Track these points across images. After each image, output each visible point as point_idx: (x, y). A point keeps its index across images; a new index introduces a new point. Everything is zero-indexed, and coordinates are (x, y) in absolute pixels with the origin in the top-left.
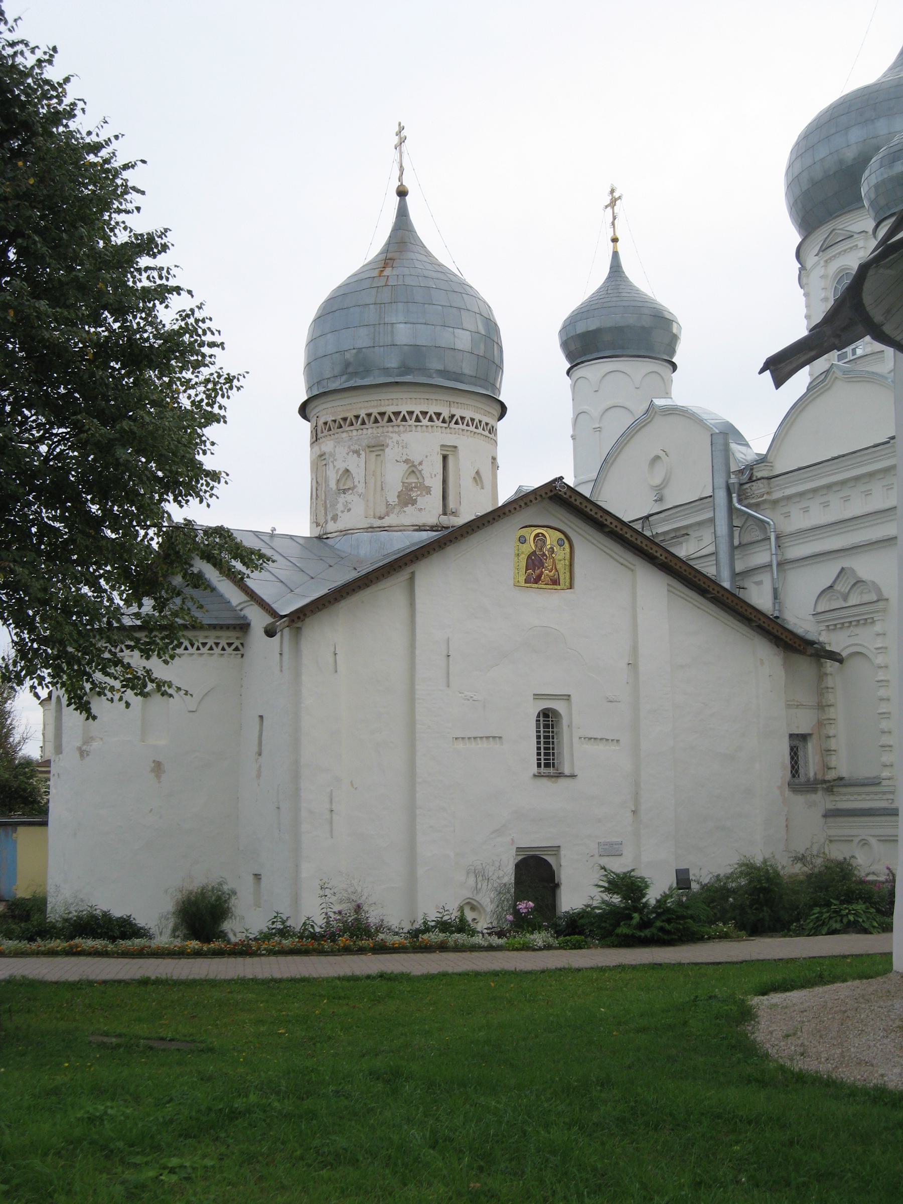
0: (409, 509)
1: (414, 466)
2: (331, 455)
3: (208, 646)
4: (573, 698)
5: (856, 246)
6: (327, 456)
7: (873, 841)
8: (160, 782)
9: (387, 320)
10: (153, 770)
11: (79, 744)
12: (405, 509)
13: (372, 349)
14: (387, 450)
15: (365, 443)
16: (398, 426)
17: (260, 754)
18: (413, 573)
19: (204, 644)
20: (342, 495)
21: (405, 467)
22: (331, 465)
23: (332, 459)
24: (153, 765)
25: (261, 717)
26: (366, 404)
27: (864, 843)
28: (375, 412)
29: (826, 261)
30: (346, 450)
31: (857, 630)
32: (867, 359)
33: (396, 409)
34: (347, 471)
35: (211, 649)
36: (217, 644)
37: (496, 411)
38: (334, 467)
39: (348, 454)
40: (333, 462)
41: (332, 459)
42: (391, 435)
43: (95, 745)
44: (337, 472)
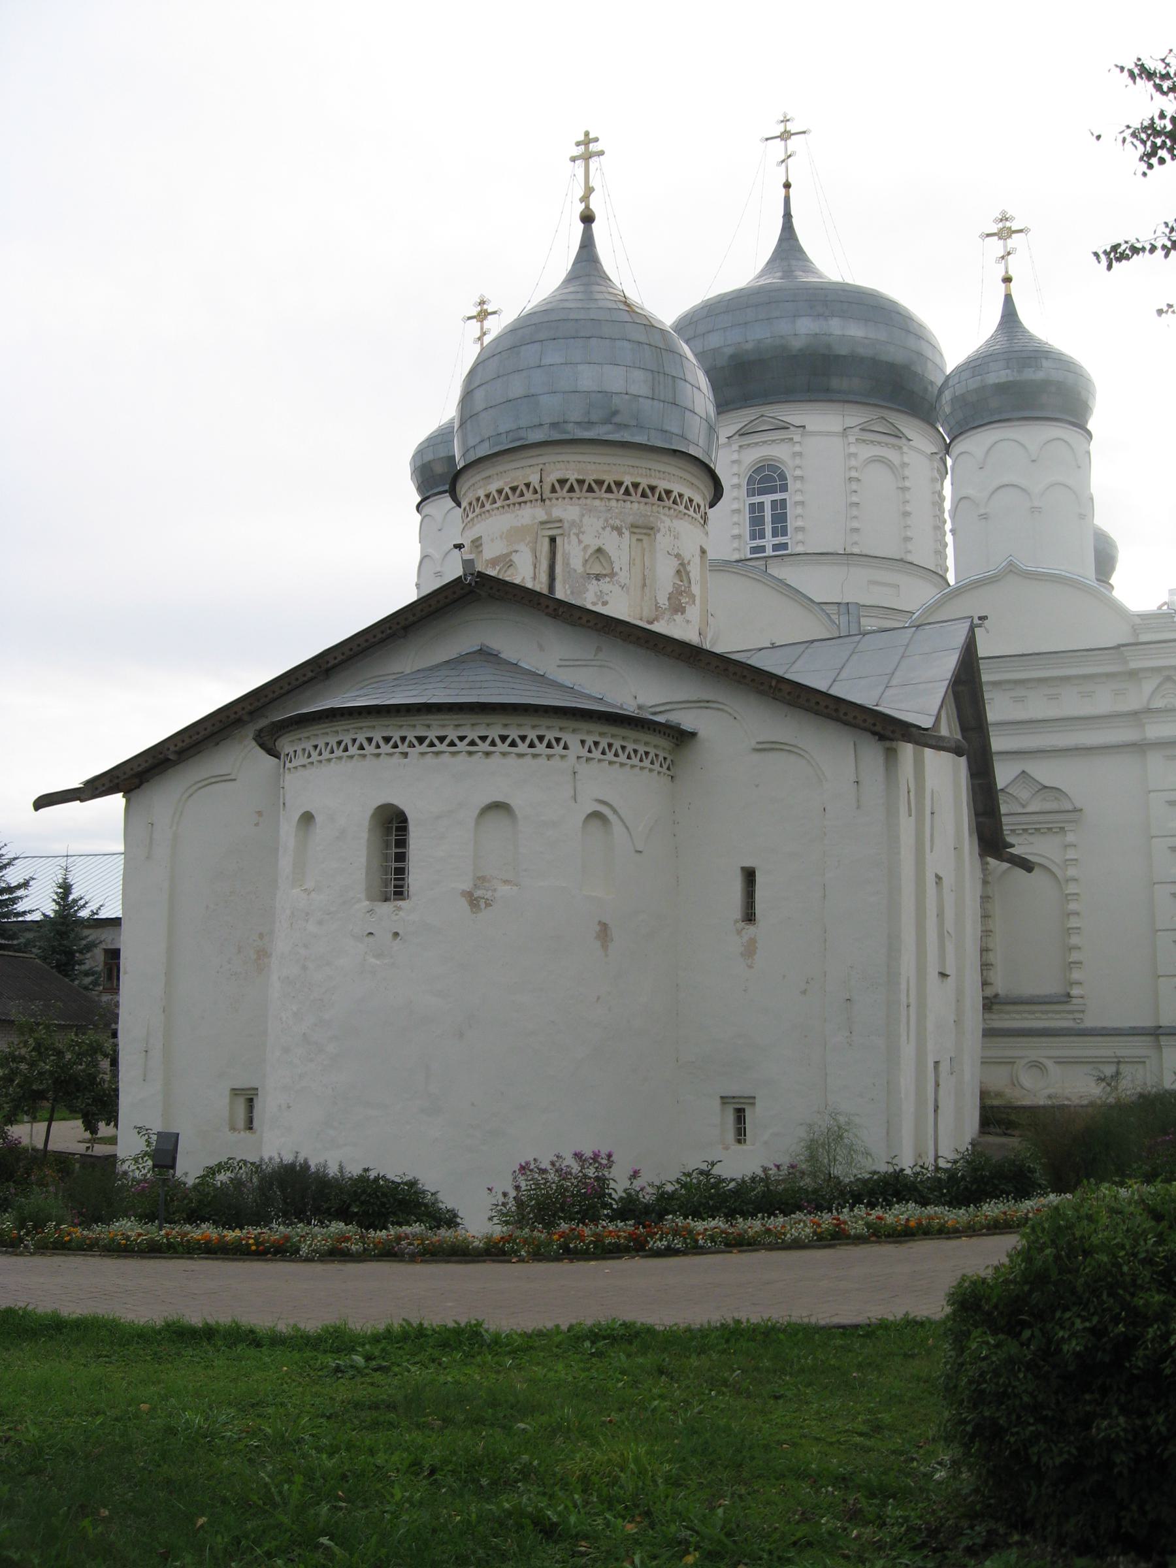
0: (678, 617)
1: (682, 564)
2: (573, 524)
6: (566, 525)
7: (1049, 1064)
11: (467, 886)
12: (675, 617)
13: (650, 401)
14: (659, 536)
15: (630, 519)
16: (670, 508)
17: (749, 916)
20: (594, 582)
23: (575, 530)
25: (750, 876)
26: (632, 470)
27: (1037, 1065)
28: (644, 482)
29: (740, 447)
30: (601, 523)
31: (1031, 839)
32: (799, 558)
34: (599, 550)
38: (580, 542)
39: (604, 528)
40: (577, 535)
41: (575, 530)
44: (586, 548)
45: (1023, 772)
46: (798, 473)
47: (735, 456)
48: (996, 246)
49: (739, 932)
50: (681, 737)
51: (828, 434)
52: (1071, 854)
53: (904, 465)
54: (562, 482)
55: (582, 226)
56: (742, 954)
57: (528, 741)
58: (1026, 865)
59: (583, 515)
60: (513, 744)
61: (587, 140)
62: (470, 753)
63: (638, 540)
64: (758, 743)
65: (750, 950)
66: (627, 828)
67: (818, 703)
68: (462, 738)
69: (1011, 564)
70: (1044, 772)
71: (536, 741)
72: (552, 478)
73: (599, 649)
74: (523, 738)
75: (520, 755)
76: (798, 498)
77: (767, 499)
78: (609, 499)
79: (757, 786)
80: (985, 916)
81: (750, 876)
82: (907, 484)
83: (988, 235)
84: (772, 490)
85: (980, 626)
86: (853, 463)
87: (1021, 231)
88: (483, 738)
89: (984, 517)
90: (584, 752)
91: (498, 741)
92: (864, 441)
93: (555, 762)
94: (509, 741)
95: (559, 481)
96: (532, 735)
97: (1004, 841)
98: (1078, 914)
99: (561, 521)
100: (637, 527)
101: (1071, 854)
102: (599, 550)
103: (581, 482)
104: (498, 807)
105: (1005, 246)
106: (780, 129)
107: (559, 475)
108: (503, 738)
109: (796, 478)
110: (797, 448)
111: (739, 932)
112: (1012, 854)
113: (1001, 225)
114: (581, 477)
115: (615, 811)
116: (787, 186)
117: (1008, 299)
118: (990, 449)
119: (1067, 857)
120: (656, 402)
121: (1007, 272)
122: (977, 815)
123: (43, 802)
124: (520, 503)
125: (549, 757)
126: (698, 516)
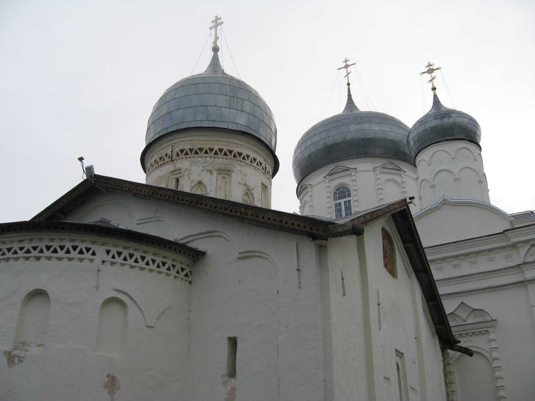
1: (249, 189)
2: (186, 170)
3: (166, 266)
5: (351, 174)
6: (183, 171)
10: (106, 386)
11: (7, 348)
13: (228, 109)
14: (233, 175)
15: (217, 166)
16: (241, 161)
17: (232, 373)
19: (164, 264)
21: (244, 188)
22: (186, 178)
23: (187, 173)
24: (106, 380)
25: (233, 342)
26: (219, 142)
28: (225, 148)
30: (201, 168)
31: (471, 338)
34: (200, 183)
36: (174, 266)
38: (189, 179)
39: (202, 171)
40: (188, 176)
41: (187, 173)
42: (236, 166)
43: (33, 350)
44: (192, 182)
45: (462, 302)
46: (355, 188)
47: (328, 185)
48: (428, 77)
49: (225, 384)
50: (197, 256)
51: (366, 171)
52: (493, 345)
53: (403, 182)
54: (182, 151)
55: (212, 53)
57: (65, 249)
58: (468, 352)
59: (192, 165)
60: (55, 251)
61: (217, 19)
62: (27, 258)
64: (240, 253)
66: (141, 310)
67: (269, 219)
68: (21, 249)
69: (444, 200)
70: (474, 302)
71: (71, 250)
72: (177, 149)
74: (62, 248)
75: (60, 259)
76: (356, 198)
77: (342, 201)
78: (206, 157)
79: (240, 282)
80: (448, 384)
81: (233, 342)
82: (405, 190)
83: (423, 73)
84: (344, 197)
85: (411, 203)
86: (379, 182)
87: (438, 69)
88: (35, 248)
89: (433, 186)
90: (109, 258)
91: (45, 249)
92: (384, 173)
93: (86, 263)
94: (52, 249)
95: (180, 151)
96: (69, 245)
97: (454, 339)
98: (502, 378)
99: (180, 169)
100: (222, 171)
101: (493, 345)
102: (200, 183)
103: (191, 150)
104: (39, 294)
105: (431, 76)
106: (349, 69)
107: (180, 148)
108: (48, 248)
110: (354, 178)
111: (225, 384)
112: (459, 346)
113: (428, 68)
114: (191, 147)
115: (131, 298)
116: (349, 84)
117: (435, 96)
118: (433, 155)
119: (492, 347)
120: (232, 110)
121: (433, 86)
122: (435, 324)
124: (163, 165)
125: (81, 260)
126: (261, 168)
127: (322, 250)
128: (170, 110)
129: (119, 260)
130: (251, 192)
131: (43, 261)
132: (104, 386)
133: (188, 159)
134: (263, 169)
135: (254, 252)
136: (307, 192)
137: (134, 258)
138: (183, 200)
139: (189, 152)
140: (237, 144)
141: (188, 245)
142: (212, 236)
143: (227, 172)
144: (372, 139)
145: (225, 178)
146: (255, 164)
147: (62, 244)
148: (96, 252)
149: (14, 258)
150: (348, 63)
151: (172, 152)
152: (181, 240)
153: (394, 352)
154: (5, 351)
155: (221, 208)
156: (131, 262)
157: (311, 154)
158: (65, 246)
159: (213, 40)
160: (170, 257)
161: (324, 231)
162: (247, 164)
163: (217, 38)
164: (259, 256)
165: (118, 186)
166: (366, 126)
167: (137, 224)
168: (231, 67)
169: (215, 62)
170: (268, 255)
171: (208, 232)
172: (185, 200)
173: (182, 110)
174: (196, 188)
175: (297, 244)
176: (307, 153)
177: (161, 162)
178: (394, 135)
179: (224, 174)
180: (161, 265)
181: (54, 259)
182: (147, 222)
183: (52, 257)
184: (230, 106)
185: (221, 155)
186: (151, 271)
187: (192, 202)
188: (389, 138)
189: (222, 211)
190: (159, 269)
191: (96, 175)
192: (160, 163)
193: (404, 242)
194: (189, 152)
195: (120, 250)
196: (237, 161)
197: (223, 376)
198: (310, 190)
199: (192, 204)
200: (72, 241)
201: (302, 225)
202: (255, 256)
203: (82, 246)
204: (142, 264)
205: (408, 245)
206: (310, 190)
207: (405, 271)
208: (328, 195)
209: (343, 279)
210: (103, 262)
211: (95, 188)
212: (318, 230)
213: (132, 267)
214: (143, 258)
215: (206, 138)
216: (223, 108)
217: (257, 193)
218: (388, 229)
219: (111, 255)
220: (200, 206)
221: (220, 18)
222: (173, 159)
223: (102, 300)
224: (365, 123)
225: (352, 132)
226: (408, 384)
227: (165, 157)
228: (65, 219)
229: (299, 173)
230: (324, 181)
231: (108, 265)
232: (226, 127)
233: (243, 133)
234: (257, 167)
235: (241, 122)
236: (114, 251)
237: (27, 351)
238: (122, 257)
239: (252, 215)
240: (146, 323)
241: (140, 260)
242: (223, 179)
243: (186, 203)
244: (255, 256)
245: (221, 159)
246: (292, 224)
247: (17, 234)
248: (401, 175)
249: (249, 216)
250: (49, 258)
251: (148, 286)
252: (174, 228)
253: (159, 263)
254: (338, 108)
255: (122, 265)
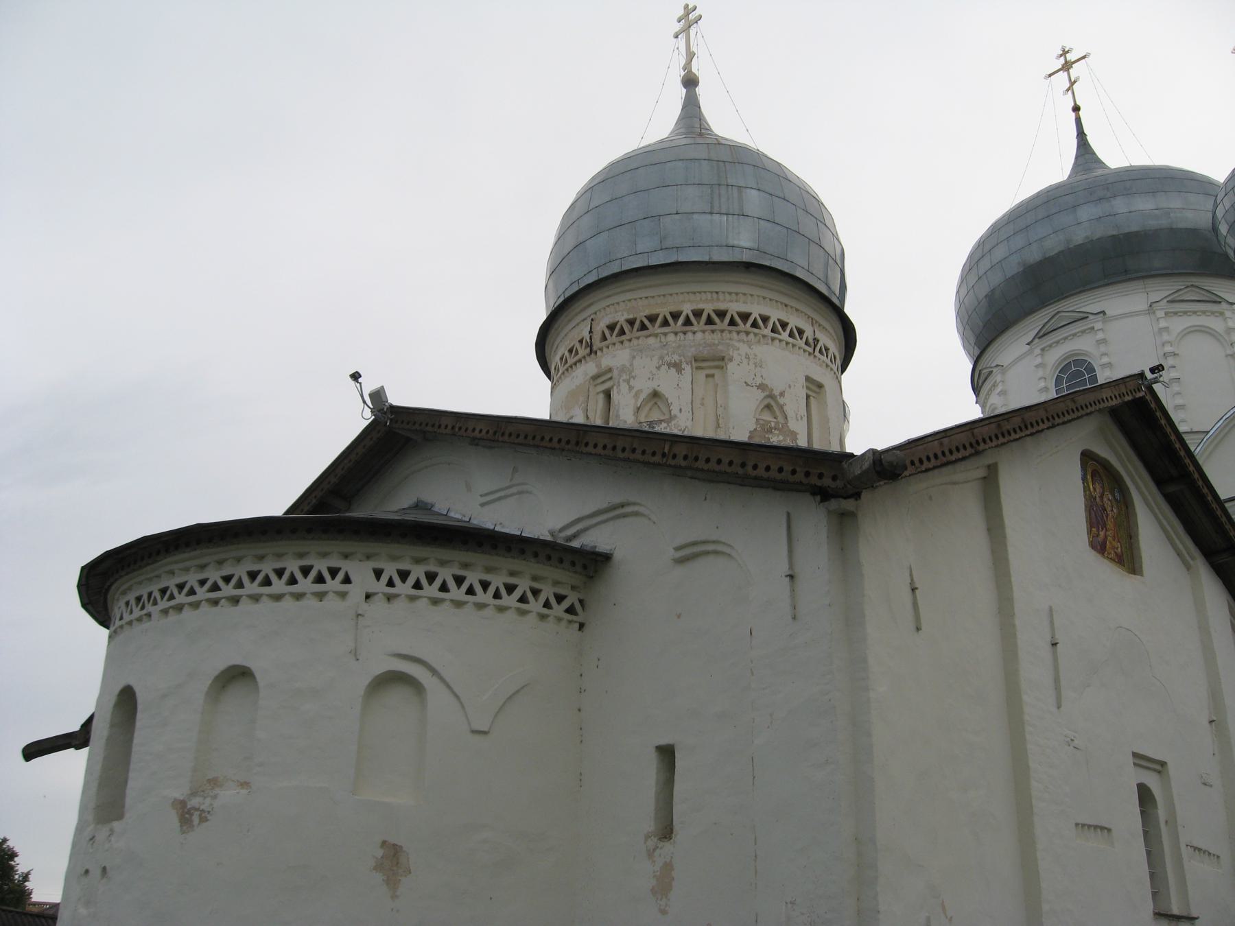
1: (771, 396)
2: (623, 369)
3: (517, 594)
4: (1171, 767)
5: (1093, 328)
6: (615, 373)
8: (394, 897)
9: (730, 181)
10: (379, 867)
11: (178, 795)
13: (708, 216)
14: (731, 367)
15: (691, 352)
16: (747, 333)
17: (666, 832)
18: (993, 470)
19: (510, 589)
21: (760, 395)
23: (625, 377)
25: (667, 754)
26: (692, 297)
28: (709, 308)
30: (655, 361)
33: (744, 308)
34: (655, 394)
35: (523, 599)
36: (536, 592)
37: (830, 341)
38: (631, 388)
39: (658, 368)
40: (628, 381)
41: (625, 377)
42: (737, 344)
43: (228, 795)
44: (637, 395)
46: (1105, 360)
47: (1039, 360)
50: (592, 564)
54: (611, 327)
56: (653, 891)
57: (286, 576)
59: (634, 357)
60: (267, 582)
61: (688, 10)
63: (707, 376)
64: (677, 549)
65: (663, 884)
71: (299, 576)
72: (601, 326)
73: (515, 470)
75: (278, 598)
78: (665, 334)
79: (679, 616)
81: (667, 754)
85: (1156, 381)
86: (1166, 337)
88: (227, 579)
90: (381, 586)
91: (246, 580)
92: (1176, 313)
93: (332, 602)
96: (293, 566)
99: (610, 370)
102: (655, 394)
103: (631, 322)
104: (237, 676)
106: (1074, 72)
107: (607, 320)
109: (1104, 366)
110: (1100, 336)
111: (650, 854)
114: (631, 316)
115: (434, 671)
116: (1076, 109)
120: (716, 217)
123: (33, 751)
126: (801, 343)
127: (844, 524)
128: (581, 239)
129: (404, 588)
130: (776, 402)
131: (246, 605)
132: (375, 868)
133: (626, 344)
134: (807, 343)
135: (704, 542)
136: (995, 385)
137: (438, 583)
138: (551, 440)
139: (626, 328)
140: (737, 294)
141: (576, 544)
142: (625, 516)
143: (716, 363)
144: (1136, 234)
145: (713, 376)
146: (785, 335)
147: (278, 565)
148: (352, 578)
149: (191, 604)
150: (1069, 57)
151: (591, 332)
152: (561, 530)
153: (1131, 760)
154: (175, 800)
155: (624, 450)
156: (432, 590)
157: (993, 291)
158: (284, 569)
159: (683, 62)
160: (525, 575)
161: (834, 478)
162: (764, 336)
163: (691, 56)
164: (716, 552)
165: (433, 426)
166: (1120, 205)
167: (482, 505)
168: (726, 121)
169: (691, 110)
170: (729, 546)
171: (614, 508)
172: (555, 440)
173: (604, 235)
174: (647, 408)
175: (788, 514)
176: (983, 291)
177: (574, 359)
178: (1192, 214)
179: (710, 367)
180: (503, 591)
181: (265, 598)
182: (500, 499)
183: (261, 595)
184: (712, 207)
185: (699, 325)
186: (481, 606)
187: (568, 442)
188: (1182, 225)
189: (626, 455)
190: (498, 602)
191: (392, 407)
192: (571, 361)
193: (1160, 482)
194: (626, 328)
195: (404, 566)
196: (738, 333)
197: (647, 837)
198: (999, 378)
199: (569, 447)
200: (301, 556)
201: (788, 468)
202: (707, 553)
203: (321, 566)
204: (457, 593)
205: (1172, 489)
206: (999, 378)
207: (1172, 553)
208: (1042, 384)
209: (913, 590)
210: (368, 596)
211: (397, 437)
212: (821, 476)
213: (435, 602)
214: (459, 580)
215: (662, 291)
216: (695, 216)
217: (794, 404)
218: (1103, 452)
219: (384, 579)
220: (585, 450)
221: (695, 8)
222: (595, 348)
223: (366, 680)
224: (1114, 196)
225: (1085, 225)
226: (1183, 840)
227: (578, 345)
228: (348, 509)
229: (972, 340)
230: (1030, 352)
231: (379, 605)
232: (706, 259)
233: (748, 267)
234: (790, 340)
235: (743, 240)
236: (390, 570)
237: (215, 797)
238: (411, 580)
239: (685, 457)
240: (469, 724)
241: (451, 584)
242: (710, 379)
243: (557, 446)
244: (707, 553)
245: (699, 335)
246: (768, 469)
247: (193, 554)
248: (1222, 314)
249: (680, 461)
250: (256, 598)
251: (472, 642)
252: (542, 507)
253: (497, 589)
254: (1056, 168)
255: (412, 598)
